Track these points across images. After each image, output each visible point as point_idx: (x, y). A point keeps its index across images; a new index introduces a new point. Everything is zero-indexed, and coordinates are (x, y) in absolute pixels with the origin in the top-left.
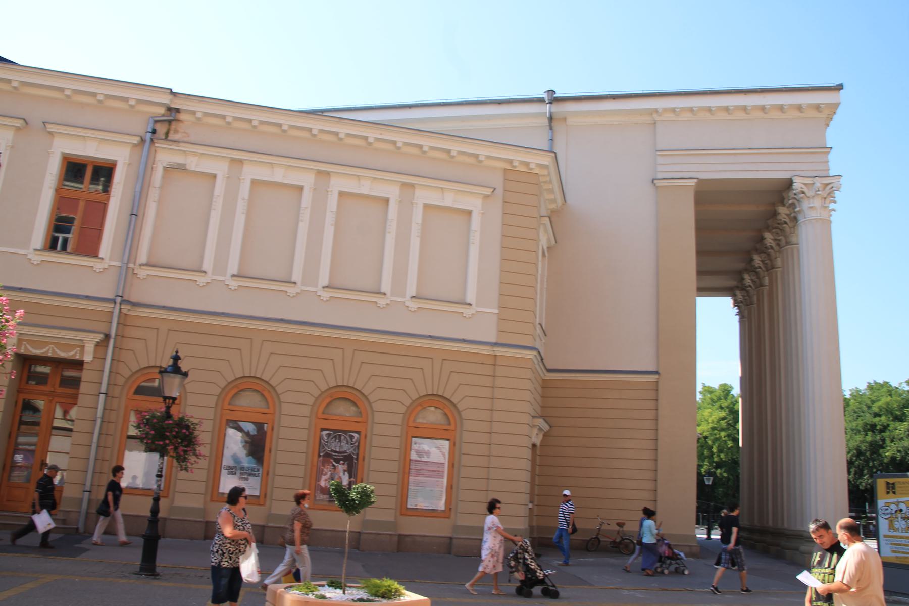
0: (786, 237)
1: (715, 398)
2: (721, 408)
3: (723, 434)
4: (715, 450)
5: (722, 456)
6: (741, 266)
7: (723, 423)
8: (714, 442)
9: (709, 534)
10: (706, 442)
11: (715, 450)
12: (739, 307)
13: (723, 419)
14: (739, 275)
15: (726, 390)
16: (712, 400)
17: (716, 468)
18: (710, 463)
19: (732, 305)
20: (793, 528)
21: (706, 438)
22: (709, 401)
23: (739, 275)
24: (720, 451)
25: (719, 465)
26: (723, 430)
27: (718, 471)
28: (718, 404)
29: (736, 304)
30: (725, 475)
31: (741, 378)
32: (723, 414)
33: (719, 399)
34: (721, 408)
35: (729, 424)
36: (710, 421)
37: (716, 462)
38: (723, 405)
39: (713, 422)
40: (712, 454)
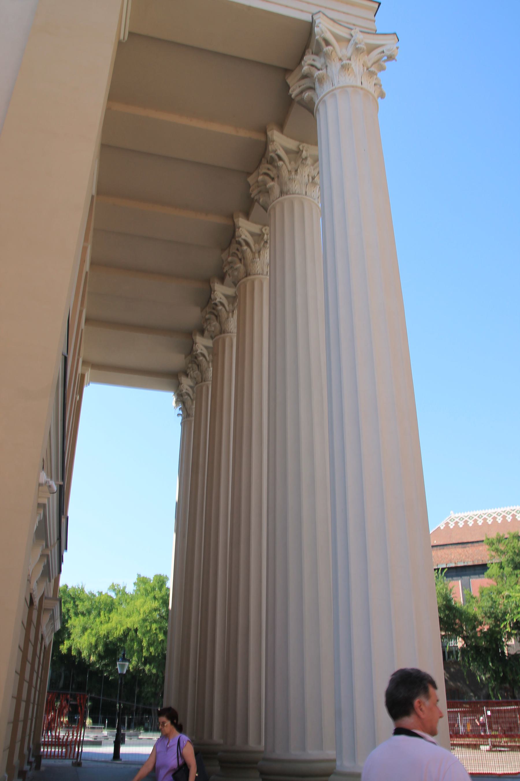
0: (281, 185)
1: (149, 589)
2: (155, 598)
3: (154, 626)
4: (145, 644)
5: (152, 649)
6: (192, 315)
7: (156, 615)
8: (144, 634)
9: (118, 742)
10: (137, 635)
11: (145, 644)
12: (184, 403)
13: (155, 610)
14: (187, 336)
15: (161, 581)
16: (146, 590)
17: (145, 664)
18: (139, 658)
19: (174, 404)
20: (279, 753)
21: (136, 630)
22: (142, 590)
23: (187, 336)
24: (150, 645)
25: (147, 661)
26: (155, 621)
27: (148, 667)
28: (152, 595)
29: (181, 399)
30: (154, 671)
31: (178, 505)
32: (156, 604)
33: (154, 589)
34: (155, 598)
35: (161, 617)
36: (142, 612)
37: (145, 657)
38: (157, 596)
39: (144, 612)
40: (142, 648)
